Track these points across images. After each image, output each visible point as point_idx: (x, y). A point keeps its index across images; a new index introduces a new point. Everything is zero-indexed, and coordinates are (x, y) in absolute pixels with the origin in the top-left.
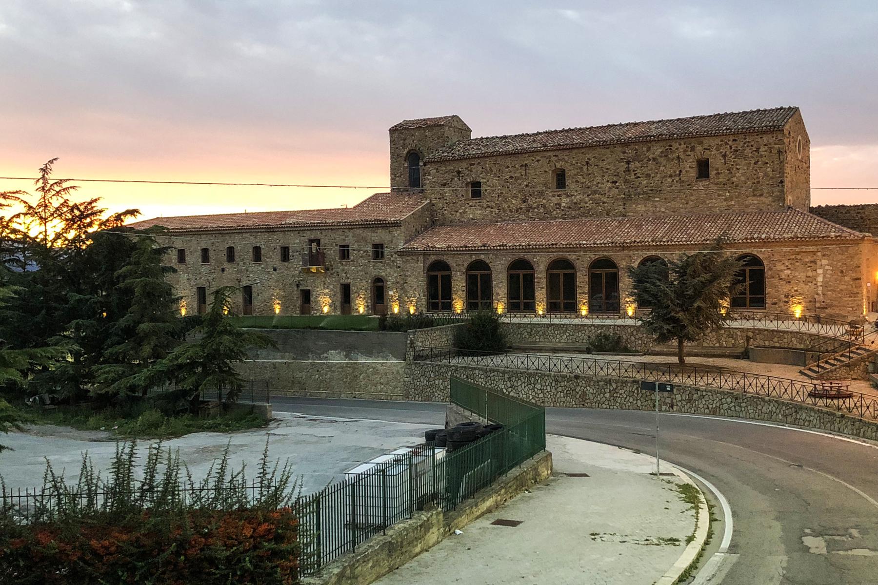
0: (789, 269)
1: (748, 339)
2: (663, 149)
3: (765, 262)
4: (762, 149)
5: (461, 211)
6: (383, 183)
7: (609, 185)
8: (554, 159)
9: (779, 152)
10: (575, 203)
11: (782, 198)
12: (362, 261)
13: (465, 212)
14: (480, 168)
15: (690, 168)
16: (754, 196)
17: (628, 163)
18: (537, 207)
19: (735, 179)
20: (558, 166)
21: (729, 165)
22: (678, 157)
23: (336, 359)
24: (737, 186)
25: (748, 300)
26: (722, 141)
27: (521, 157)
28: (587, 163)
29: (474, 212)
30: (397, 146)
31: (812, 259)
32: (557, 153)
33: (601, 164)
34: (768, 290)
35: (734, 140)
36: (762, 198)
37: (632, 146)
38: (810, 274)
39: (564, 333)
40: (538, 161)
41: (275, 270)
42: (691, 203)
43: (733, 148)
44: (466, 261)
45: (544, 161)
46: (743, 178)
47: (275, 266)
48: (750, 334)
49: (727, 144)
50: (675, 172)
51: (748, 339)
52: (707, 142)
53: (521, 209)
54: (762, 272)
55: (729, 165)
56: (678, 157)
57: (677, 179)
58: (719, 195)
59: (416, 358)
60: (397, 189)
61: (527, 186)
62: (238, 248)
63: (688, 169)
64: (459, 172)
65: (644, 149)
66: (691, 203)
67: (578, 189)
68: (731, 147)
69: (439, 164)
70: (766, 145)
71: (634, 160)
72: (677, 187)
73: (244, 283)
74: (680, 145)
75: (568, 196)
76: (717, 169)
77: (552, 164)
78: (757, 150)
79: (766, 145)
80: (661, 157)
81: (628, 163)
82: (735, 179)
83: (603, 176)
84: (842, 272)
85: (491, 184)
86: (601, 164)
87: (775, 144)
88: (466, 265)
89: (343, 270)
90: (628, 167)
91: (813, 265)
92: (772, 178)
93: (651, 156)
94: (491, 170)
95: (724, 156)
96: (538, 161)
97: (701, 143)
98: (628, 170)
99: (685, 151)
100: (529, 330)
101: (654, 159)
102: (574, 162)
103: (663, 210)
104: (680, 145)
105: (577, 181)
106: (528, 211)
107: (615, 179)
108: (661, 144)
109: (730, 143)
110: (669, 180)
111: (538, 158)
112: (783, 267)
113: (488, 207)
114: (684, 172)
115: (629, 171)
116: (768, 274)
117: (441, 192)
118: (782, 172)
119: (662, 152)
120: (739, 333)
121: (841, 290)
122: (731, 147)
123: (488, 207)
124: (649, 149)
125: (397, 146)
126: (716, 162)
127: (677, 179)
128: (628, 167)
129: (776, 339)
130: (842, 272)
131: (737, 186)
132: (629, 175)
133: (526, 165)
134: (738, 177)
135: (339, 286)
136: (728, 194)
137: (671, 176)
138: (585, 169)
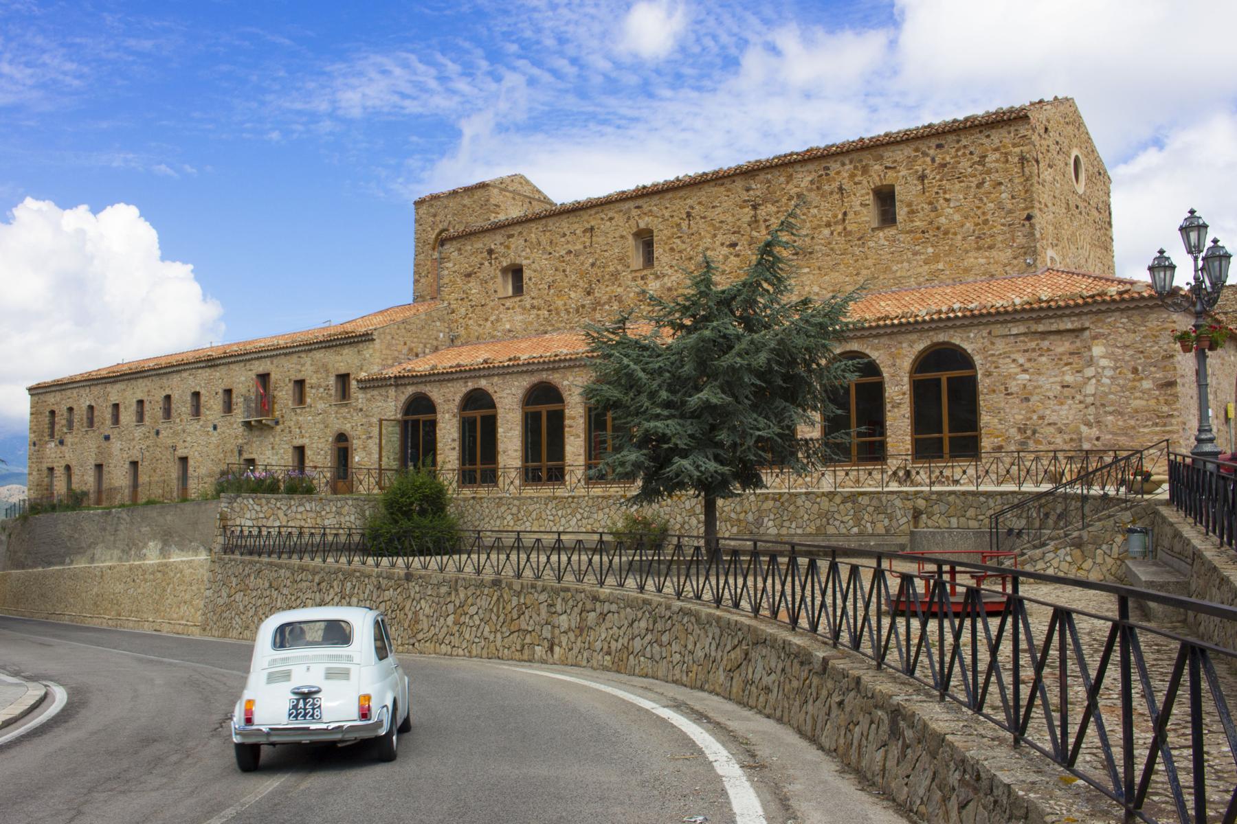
0: (1025, 371)
1: (917, 514)
2: (814, 176)
3: (978, 360)
4: (992, 157)
5: (493, 318)
6: (403, 292)
7: (725, 251)
8: (635, 212)
9: (1023, 159)
10: (670, 289)
11: (1030, 250)
12: (321, 406)
13: (498, 320)
14: (521, 241)
15: (865, 214)
16: (979, 249)
17: (755, 207)
18: (609, 302)
19: (943, 220)
20: (642, 225)
21: (931, 193)
22: (841, 189)
23: (152, 556)
24: (946, 233)
25: (946, 443)
26: (917, 150)
27: (585, 215)
28: (689, 215)
29: (513, 319)
30: (424, 227)
31: (1073, 348)
32: (640, 202)
33: (710, 214)
34: (985, 418)
35: (939, 146)
36: (994, 253)
37: (762, 177)
38: (1069, 378)
39: (573, 514)
40: (611, 219)
41: (215, 428)
42: (864, 272)
43: (938, 160)
44: (458, 391)
45: (619, 219)
46: (957, 217)
47: (216, 422)
48: (921, 503)
49: (925, 154)
50: (835, 216)
51: (917, 514)
52: (890, 155)
53: (583, 306)
54: (972, 382)
55: (931, 193)
56: (841, 189)
57: (840, 228)
58: (915, 254)
59: (228, 549)
60: (418, 298)
61: (593, 265)
62: (175, 397)
63: (858, 208)
64: (490, 252)
65: (782, 179)
66: (864, 272)
67: (674, 263)
68: (933, 160)
69: (462, 241)
70: (997, 149)
71: (765, 201)
72: (839, 242)
73: (181, 452)
74: (843, 164)
75: (657, 277)
76: (909, 205)
77: (632, 222)
78: (982, 160)
79: (997, 149)
80: (810, 190)
81: (755, 207)
82: (943, 220)
83: (715, 236)
84: (1135, 371)
85: (536, 265)
86: (710, 214)
87: (1014, 145)
88: (458, 399)
89: (297, 422)
90: (755, 216)
91: (1075, 359)
92: (1010, 212)
93: (794, 191)
94: (539, 243)
95: (922, 178)
96: (611, 219)
97: (880, 158)
98: (755, 220)
99: (852, 176)
100: (514, 510)
101: (799, 196)
102: (667, 215)
103: (816, 289)
104: (843, 164)
105: (672, 249)
106: (594, 310)
107: (734, 238)
108: (811, 167)
109: (932, 152)
110: (826, 232)
111: (611, 214)
112: (1014, 369)
113: (533, 307)
114: (851, 216)
115: (756, 221)
116: (983, 383)
117: (465, 288)
118: (1029, 199)
119: (812, 182)
120: (898, 503)
121: (1136, 411)
122: (933, 160)
123: (533, 307)
124: (790, 178)
125: (424, 227)
126: (907, 192)
127: (840, 228)
128: (755, 216)
129: (971, 512)
130: (1135, 371)
131: (946, 233)
132: (757, 229)
133: (592, 229)
134: (949, 216)
135: (291, 450)
136: (930, 250)
137: (828, 225)
138: (684, 225)
